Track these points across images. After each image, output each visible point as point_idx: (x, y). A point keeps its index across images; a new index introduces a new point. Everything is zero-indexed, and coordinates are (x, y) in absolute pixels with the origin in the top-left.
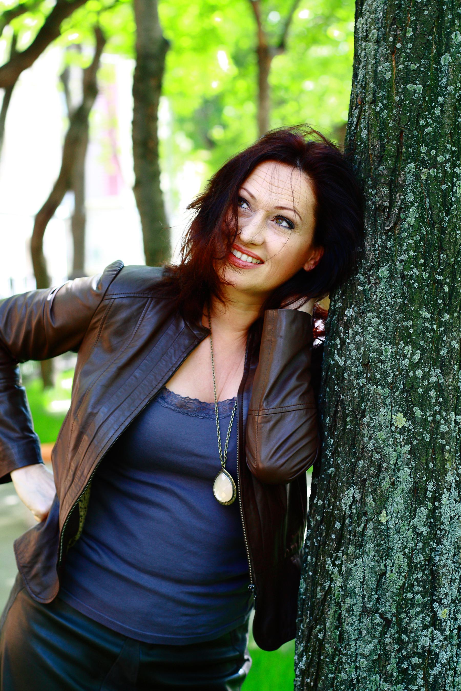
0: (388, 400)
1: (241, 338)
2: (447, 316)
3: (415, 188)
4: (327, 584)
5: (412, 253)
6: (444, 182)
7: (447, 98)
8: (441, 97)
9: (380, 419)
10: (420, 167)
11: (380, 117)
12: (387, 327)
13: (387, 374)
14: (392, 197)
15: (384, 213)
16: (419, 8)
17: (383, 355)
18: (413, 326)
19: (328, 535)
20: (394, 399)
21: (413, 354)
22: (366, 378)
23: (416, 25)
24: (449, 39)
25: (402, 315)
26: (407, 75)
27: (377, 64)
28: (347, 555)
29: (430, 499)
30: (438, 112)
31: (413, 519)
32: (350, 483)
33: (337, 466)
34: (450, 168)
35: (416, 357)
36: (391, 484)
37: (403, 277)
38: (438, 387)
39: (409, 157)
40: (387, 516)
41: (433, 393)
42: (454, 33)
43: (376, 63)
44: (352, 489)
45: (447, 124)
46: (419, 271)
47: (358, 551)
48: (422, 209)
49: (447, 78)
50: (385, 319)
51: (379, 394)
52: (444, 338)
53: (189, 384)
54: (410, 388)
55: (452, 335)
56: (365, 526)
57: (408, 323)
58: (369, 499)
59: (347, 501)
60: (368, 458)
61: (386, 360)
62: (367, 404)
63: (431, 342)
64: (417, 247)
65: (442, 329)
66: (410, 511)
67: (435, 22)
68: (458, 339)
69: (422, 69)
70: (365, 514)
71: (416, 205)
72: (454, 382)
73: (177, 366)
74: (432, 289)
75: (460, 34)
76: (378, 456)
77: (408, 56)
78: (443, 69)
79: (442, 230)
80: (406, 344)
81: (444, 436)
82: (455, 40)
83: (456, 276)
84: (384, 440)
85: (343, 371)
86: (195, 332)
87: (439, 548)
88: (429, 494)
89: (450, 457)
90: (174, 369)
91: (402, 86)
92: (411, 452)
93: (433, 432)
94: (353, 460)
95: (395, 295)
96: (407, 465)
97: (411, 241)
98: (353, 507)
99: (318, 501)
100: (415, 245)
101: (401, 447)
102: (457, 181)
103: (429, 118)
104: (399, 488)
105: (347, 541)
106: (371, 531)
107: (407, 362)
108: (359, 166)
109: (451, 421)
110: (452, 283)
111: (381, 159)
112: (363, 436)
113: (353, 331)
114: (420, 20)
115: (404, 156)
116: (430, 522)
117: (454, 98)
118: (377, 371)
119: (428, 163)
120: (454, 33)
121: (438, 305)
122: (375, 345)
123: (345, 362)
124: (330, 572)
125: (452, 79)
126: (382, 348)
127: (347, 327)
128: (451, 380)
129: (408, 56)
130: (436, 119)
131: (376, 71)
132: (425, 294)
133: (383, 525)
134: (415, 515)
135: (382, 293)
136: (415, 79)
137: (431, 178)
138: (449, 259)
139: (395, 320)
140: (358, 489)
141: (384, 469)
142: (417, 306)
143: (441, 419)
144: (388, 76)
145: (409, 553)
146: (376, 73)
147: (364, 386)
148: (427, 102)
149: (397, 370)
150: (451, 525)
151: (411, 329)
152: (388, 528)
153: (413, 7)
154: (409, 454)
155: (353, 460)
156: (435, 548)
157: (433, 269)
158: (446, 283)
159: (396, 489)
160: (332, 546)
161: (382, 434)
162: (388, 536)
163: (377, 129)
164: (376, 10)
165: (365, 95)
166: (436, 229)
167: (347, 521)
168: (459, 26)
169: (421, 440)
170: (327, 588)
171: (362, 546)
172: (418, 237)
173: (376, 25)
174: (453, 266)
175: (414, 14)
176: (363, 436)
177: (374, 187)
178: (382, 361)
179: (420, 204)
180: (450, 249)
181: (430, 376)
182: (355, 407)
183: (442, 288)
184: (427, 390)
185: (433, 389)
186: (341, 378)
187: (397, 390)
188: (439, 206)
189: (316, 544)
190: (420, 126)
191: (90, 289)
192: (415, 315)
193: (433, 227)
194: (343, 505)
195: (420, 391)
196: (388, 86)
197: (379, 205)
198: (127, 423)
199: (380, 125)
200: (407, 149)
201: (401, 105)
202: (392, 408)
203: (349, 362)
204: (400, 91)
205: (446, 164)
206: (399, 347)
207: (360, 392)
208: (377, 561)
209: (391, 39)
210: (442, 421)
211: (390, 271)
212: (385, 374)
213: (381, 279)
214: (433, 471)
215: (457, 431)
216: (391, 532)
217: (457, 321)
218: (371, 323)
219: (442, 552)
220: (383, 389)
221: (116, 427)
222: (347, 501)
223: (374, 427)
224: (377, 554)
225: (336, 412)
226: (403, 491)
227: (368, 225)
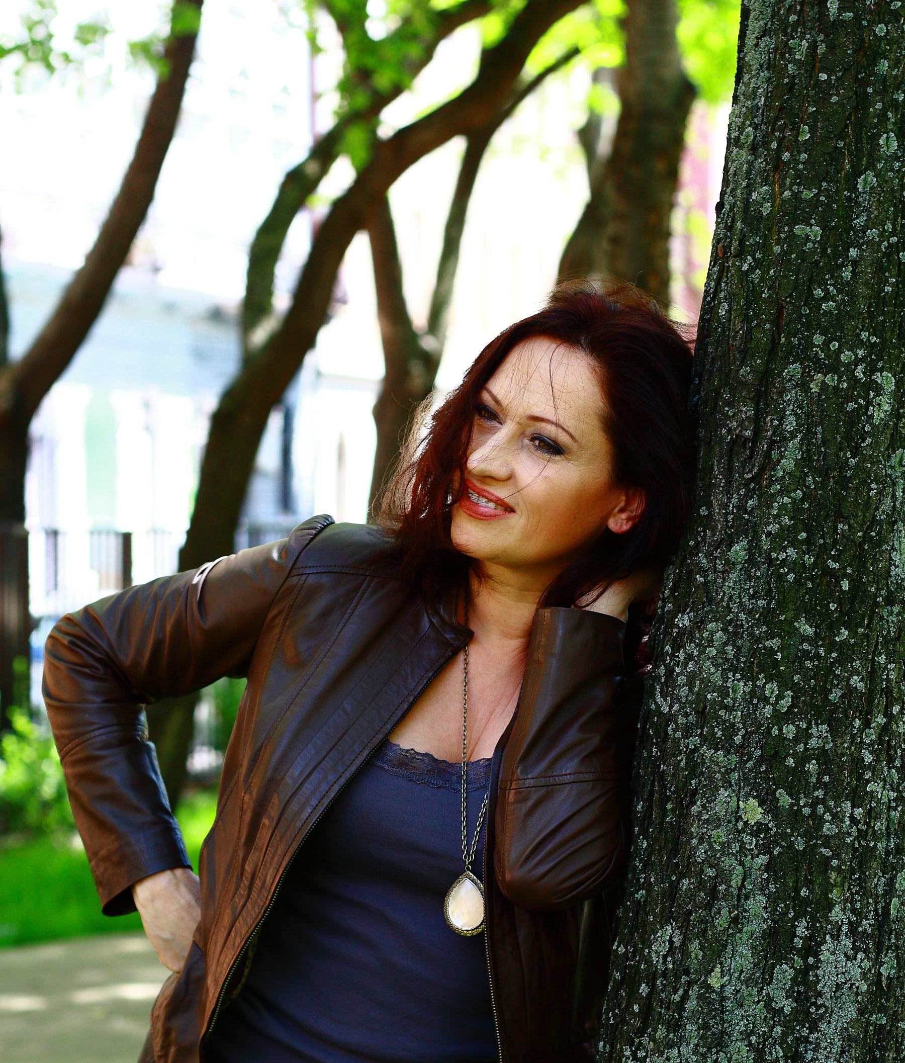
0: (735, 776)
1: (517, 652)
2: (845, 633)
3: (800, 407)
5: (786, 520)
6: (849, 398)
7: (864, 250)
8: (854, 248)
9: (719, 808)
10: (810, 371)
11: (747, 280)
12: (739, 649)
13: (734, 730)
14: (760, 422)
15: (745, 448)
16: (823, 92)
17: (728, 696)
18: (781, 649)
19: (630, 1005)
20: (744, 773)
21: (780, 697)
22: (700, 735)
23: (816, 121)
24: (875, 146)
25: (764, 629)
26: (796, 209)
27: (749, 189)
28: (654, 1041)
29: (799, 951)
30: (847, 274)
31: (768, 985)
32: (666, 918)
33: (648, 886)
34: (863, 373)
35: (786, 703)
36: (731, 922)
37: (770, 562)
38: (822, 755)
39: (791, 353)
40: (723, 976)
41: (812, 766)
42: (885, 135)
43: (748, 186)
44: (669, 928)
45: (863, 297)
46: (797, 553)
47: (671, 1036)
48: (808, 445)
49: (867, 216)
50: (735, 634)
51: (717, 764)
52: (838, 672)
53: (426, 734)
54: (772, 756)
55: (852, 666)
56: (686, 992)
57: (774, 643)
58: (694, 946)
59: (661, 949)
60: (696, 875)
61: (733, 706)
62: (700, 780)
63: (812, 678)
64: (795, 510)
65: (834, 655)
66: (764, 970)
67: (850, 114)
68: (864, 673)
69: (822, 198)
70: (687, 972)
71: (799, 436)
72: (853, 748)
73: (416, 693)
74: (818, 585)
75: (895, 138)
76: (711, 872)
77: (799, 175)
78: (861, 199)
79: (843, 482)
80: (769, 679)
81: (829, 842)
82: (885, 148)
83: (865, 563)
84: (722, 844)
85: (667, 723)
86: (448, 636)
87: (813, 1037)
88: (798, 943)
89: (839, 880)
90: (411, 698)
91: (786, 229)
92: (768, 868)
93: (811, 835)
94: (674, 878)
95: (755, 593)
96: (761, 889)
97: (786, 500)
98: (669, 959)
99: (618, 946)
100: (793, 507)
101: (752, 858)
102: (877, 396)
103: (830, 285)
104: (745, 929)
105: (657, 1017)
106: (695, 1002)
107: (768, 710)
108: (712, 366)
109: (844, 816)
110: (858, 575)
111: (745, 355)
112: (691, 837)
113: (685, 652)
114: (824, 113)
115: (782, 351)
116: (799, 991)
117: (879, 250)
118: (718, 723)
119: (824, 363)
120: (885, 135)
121: (829, 613)
122: (717, 678)
123: (671, 707)
125: (877, 217)
126: (728, 685)
127: (677, 647)
128: (846, 745)
129: (799, 175)
130: (842, 287)
131: (747, 200)
132: (806, 593)
133: (714, 991)
134: (771, 978)
135: (733, 589)
136: (808, 217)
137: (827, 390)
138: (854, 534)
139: (753, 637)
140: (680, 928)
141: (721, 896)
142: (791, 614)
143: (824, 813)
144: (766, 209)
145: (759, 1044)
146: (747, 203)
147: (696, 749)
148: (828, 256)
149: (752, 724)
150: (837, 998)
151: (779, 654)
152: (723, 999)
153: (812, 90)
154: (766, 871)
155: (674, 878)
156: (807, 1038)
157: (824, 549)
158: (845, 575)
159: (741, 931)
160: (633, 1025)
161: (720, 835)
162: (722, 1012)
163: (742, 302)
164: (754, 92)
165: (730, 242)
166: (831, 480)
167: (658, 982)
168: (894, 124)
169: (787, 847)
171: (680, 1027)
172: (799, 494)
173: (753, 119)
174: (861, 545)
175: (814, 102)
176: (691, 837)
177: (730, 404)
178: (726, 708)
179: (805, 435)
180: (856, 516)
181: (811, 736)
182: (681, 785)
183: (838, 583)
184: (803, 759)
185: (813, 759)
186: (662, 734)
187: (749, 759)
188: (839, 440)
189: (612, 1022)
190: (814, 299)
191: (269, 560)
192: (786, 628)
193: (826, 477)
194: (653, 955)
195: (791, 762)
196: (765, 227)
197: (737, 436)
198: (332, 794)
199: (747, 295)
200: (788, 338)
201: (782, 260)
202: (740, 789)
203: (676, 707)
204: (783, 236)
205: (856, 366)
206: (758, 683)
207: (688, 760)
208: (702, 1054)
209: (774, 145)
210: (827, 816)
211: (749, 550)
212: (731, 729)
213: (734, 564)
214: (806, 901)
215: (855, 834)
216: (728, 1004)
217: (863, 643)
218: (712, 641)
219: (818, 1046)
220: (725, 756)
221: (314, 802)
222: (661, 949)
223: (707, 821)
225: (652, 792)
226: (752, 935)
227: (719, 469)
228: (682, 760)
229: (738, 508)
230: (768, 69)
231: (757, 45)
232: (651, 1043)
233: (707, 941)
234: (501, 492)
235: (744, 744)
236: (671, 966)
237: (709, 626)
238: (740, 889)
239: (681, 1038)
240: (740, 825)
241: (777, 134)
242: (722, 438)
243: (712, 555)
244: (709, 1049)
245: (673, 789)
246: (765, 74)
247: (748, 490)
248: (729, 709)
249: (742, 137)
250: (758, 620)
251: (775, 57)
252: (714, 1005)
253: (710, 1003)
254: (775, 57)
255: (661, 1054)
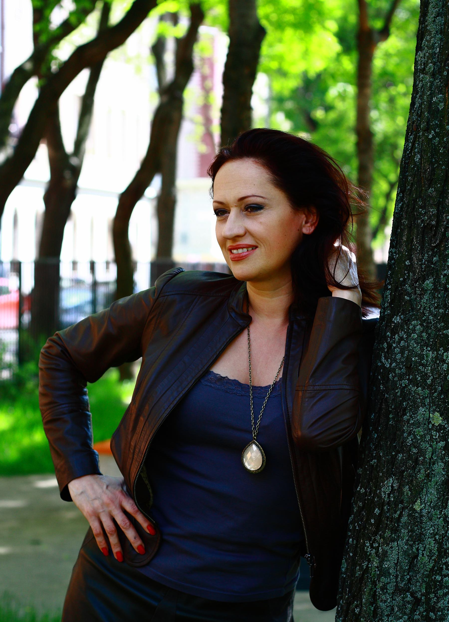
4: (365, 564)
11: (432, 143)
12: (429, 334)
13: (427, 376)
17: (424, 359)
19: (368, 520)
20: (432, 399)
22: (408, 379)
27: (432, 95)
28: (384, 538)
31: (445, 509)
32: (389, 475)
33: (379, 458)
36: (425, 476)
40: (421, 505)
43: (430, 94)
47: (393, 535)
51: (418, 394)
56: (401, 513)
59: (387, 490)
62: (408, 403)
66: (442, 501)
70: (402, 502)
76: (415, 451)
84: (421, 436)
92: (445, 448)
95: (438, 305)
96: (441, 459)
98: (392, 495)
99: (360, 489)
101: (437, 443)
104: (433, 480)
111: (431, 183)
112: (403, 432)
113: (399, 336)
122: (418, 350)
123: (391, 364)
124: (368, 554)
127: (393, 334)
133: (417, 512)
134: (447, 505)
135: (426, 303)
140: (397, 479)
144: (441, 106)
145: (440, 539)
146: (430, 103)
149: (436, 374)
154: (444, 450)
159: (431, 481)
161: (420, 431)
162: (421, 523)
165: (420, 123)
170: (365, 567)
171: (398, 531)
176: (403, 432)
177: (423, 207)
178: (423, 365)
189: (357, 528)
194: (382, 494)
197: (427, 224)
203: (394, 364)
207: (402, 392)
208: (410, 545)
211: (434, 283)
212: (425, 376)
213: (426, 290)
220: (422, 390)
222: (387, 490)
224: (410, 539)
226: (437, 483)
228: (398, 392)
229: (428, 261)
230: (441, 33)
231: (434, 21)
232: (382, 539)
233: (413, 486)
234: (248, 241)
235: (432, 384)
236: (393, 499)
237: (413, 323)
238: (430, 459)
239: (398, 537)
240: (430, 426)
241: (447, 67)
242: (418, 225)
243: (413, 285)
244: (414, 542)
245: (393, 407)
246: (439, 36)
247: (433, 252)
248: (424, 366)
249: (427, 69)
250: (439, 319)
251: (445, 28)
252: (416, 520)
253: (415, 518)
254: (445, 28)
255: (388, 545)
